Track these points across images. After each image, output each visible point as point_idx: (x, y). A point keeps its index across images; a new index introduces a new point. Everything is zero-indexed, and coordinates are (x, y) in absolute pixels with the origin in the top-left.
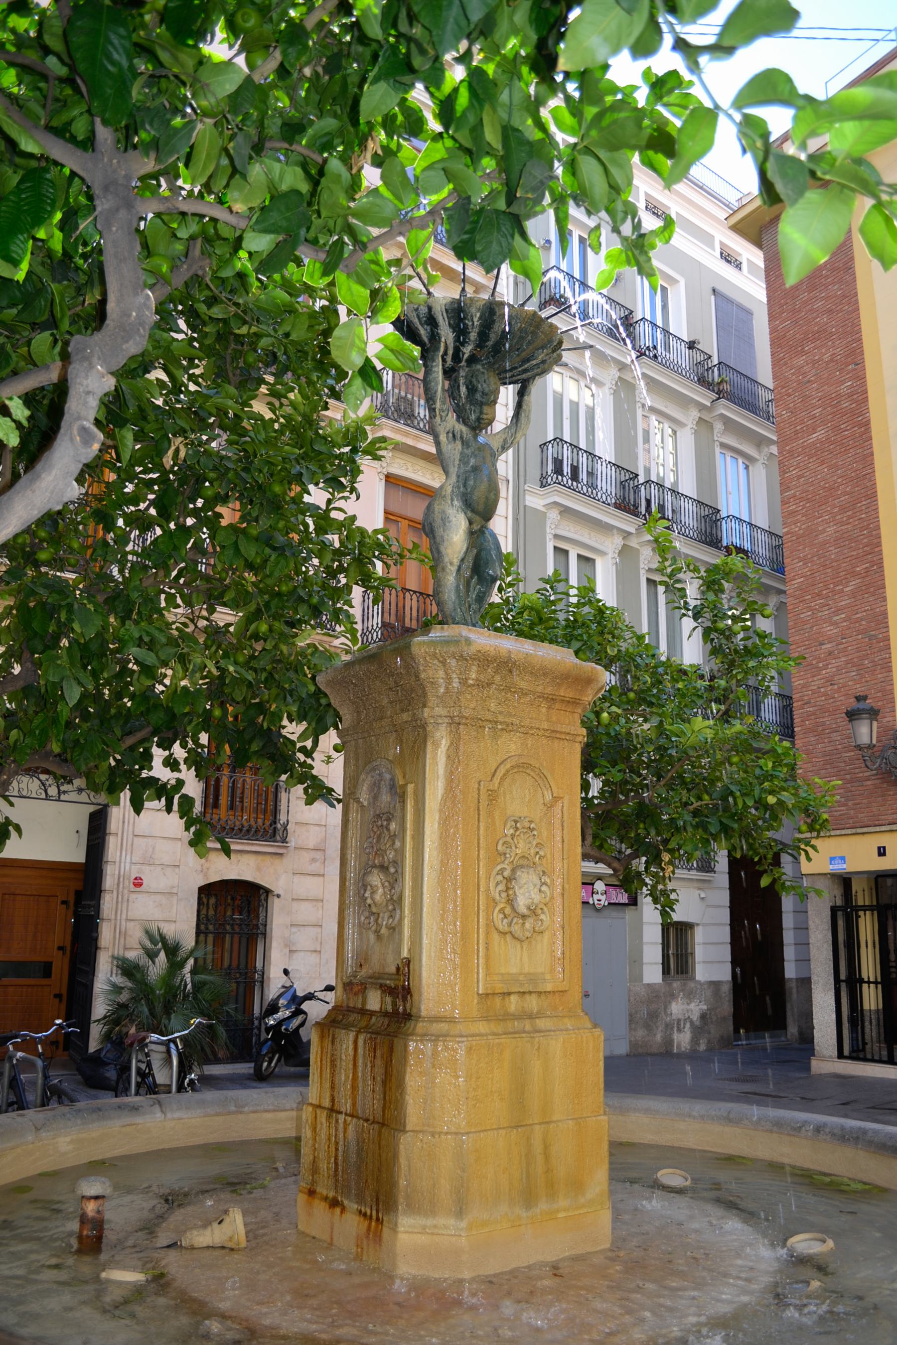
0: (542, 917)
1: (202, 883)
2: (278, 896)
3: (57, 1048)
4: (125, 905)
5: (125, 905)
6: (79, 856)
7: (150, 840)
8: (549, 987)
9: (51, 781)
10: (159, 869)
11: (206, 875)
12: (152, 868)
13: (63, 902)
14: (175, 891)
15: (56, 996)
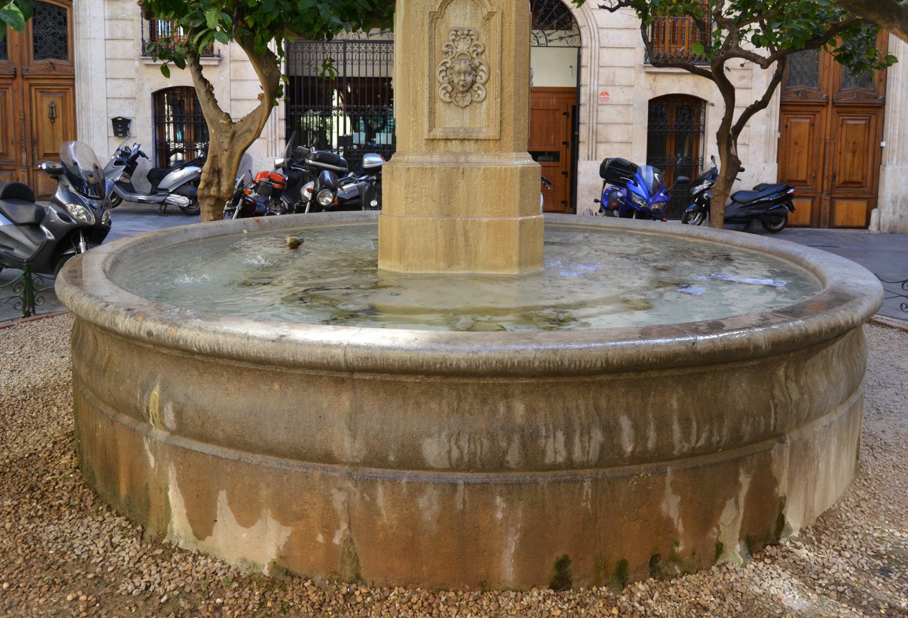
0: (479, 92)
1: (651, 97)
2: (712, 105)
3: (566, 205)
4: (595, 113)
5: (595, 113)
6: (575, 85)
7: (611, 69)
8: (482, 136)
9: (541, 34)
10: (618, 88)
11: (654, 92)
12: (614, 88)
13: (564, 114)
14: (631, 103)
15: (563, 173)
